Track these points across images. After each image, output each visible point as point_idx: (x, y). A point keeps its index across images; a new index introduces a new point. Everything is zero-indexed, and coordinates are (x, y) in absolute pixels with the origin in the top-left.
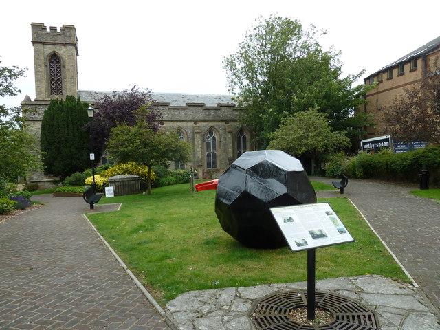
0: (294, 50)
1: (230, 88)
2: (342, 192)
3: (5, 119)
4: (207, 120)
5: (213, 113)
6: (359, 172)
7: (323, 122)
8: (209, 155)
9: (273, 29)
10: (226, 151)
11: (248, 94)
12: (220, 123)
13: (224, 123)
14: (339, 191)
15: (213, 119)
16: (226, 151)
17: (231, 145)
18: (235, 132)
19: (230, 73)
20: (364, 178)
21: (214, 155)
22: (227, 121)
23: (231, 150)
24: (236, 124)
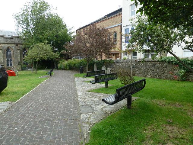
0: (46, 13)
1: (17, 29)
2: (51, 76)
3: (188, 38)
4: (6, 44)
5: (9, 40)
6: (68, 68)
7: (48, 48)
8: (8, 60)
9: (37, 4)
10: (16, 58)
11: (27, 33)
12: (13, 45)
13: (15, 45)
14: (50, 75)
15: (4, 42)
16: (16, 58)
17: (20, 55)
18: (21, 49)
19: (16, 21)
20: (70, 70)
21: (11, 60)
22: (17, 44)
23: (19, 58)
24: (21, 46)
